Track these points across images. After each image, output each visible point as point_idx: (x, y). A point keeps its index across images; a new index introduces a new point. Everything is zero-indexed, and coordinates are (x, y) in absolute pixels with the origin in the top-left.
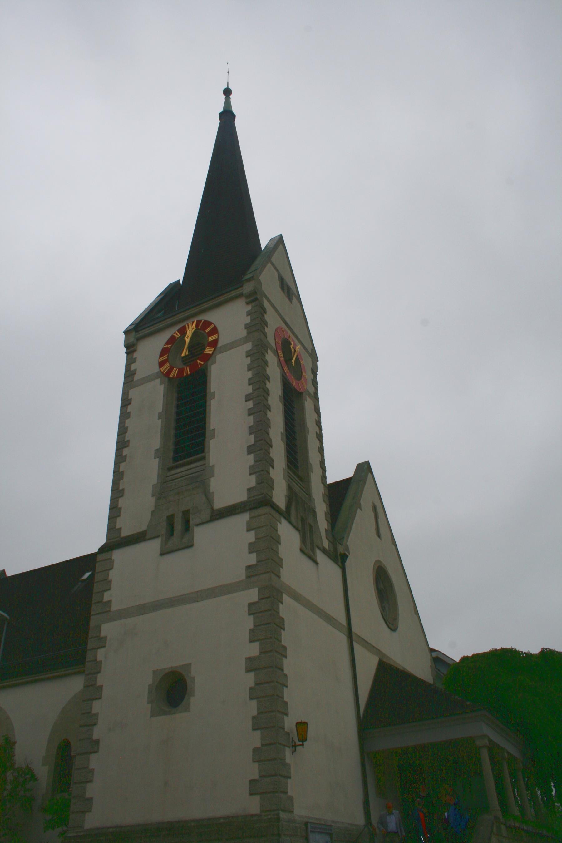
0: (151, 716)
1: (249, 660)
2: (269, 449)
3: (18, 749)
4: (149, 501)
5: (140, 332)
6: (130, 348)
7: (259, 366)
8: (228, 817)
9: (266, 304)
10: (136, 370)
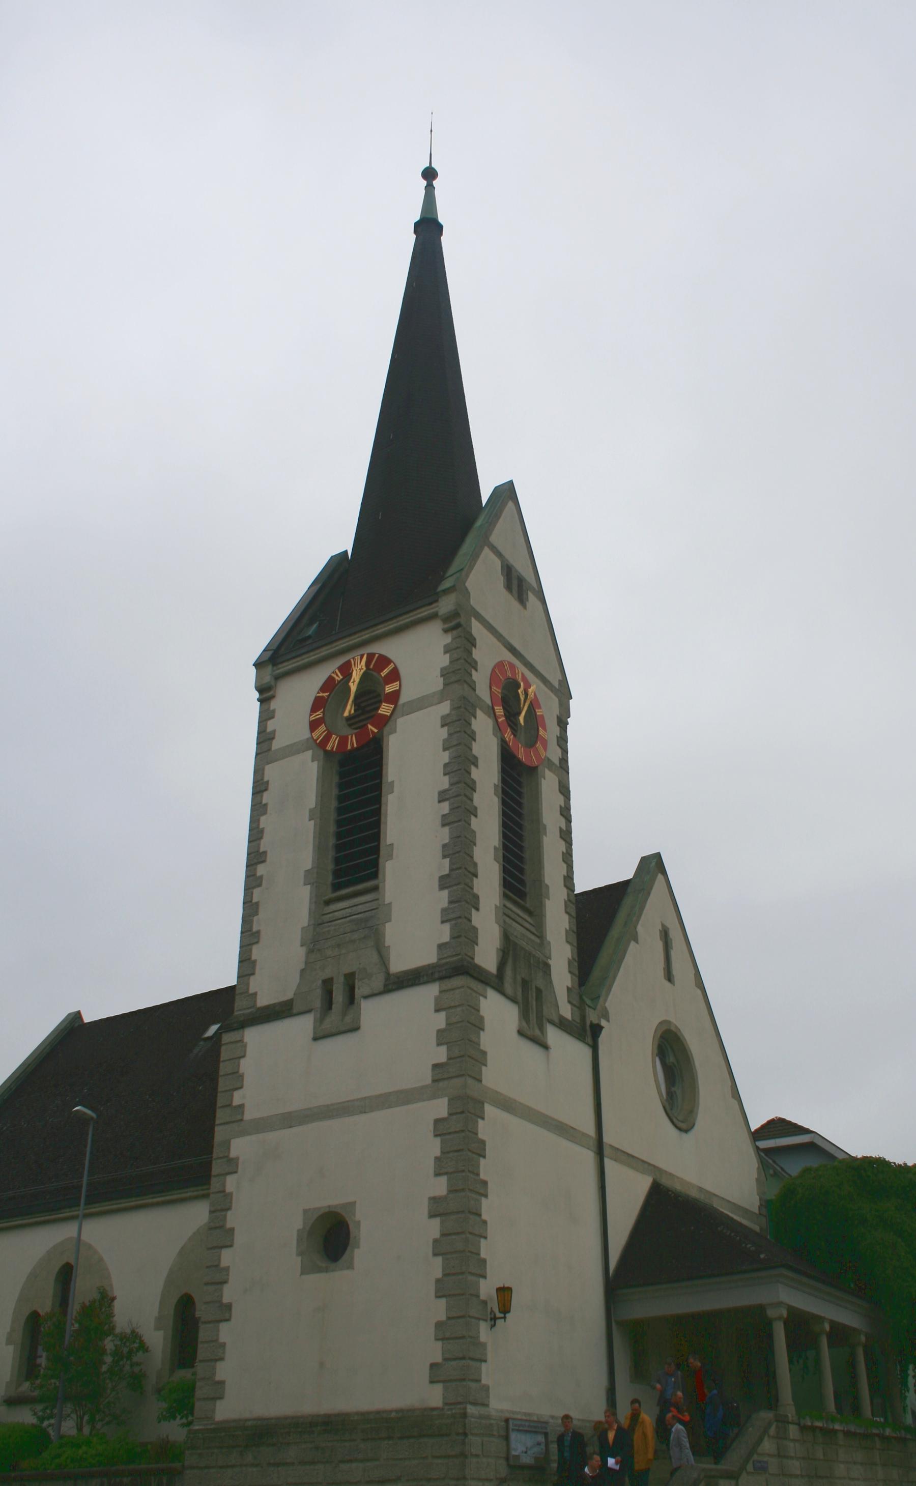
0: (302, 1273)
1: (434, 1200)
2: (472, 881)
3: (117, 1306)
4: (297, 954)
5: (280, 666)
6: (266, 693)
7: (460, 744)
8: (402, 1410)
9: (477, 628)
10: (274, 731)
